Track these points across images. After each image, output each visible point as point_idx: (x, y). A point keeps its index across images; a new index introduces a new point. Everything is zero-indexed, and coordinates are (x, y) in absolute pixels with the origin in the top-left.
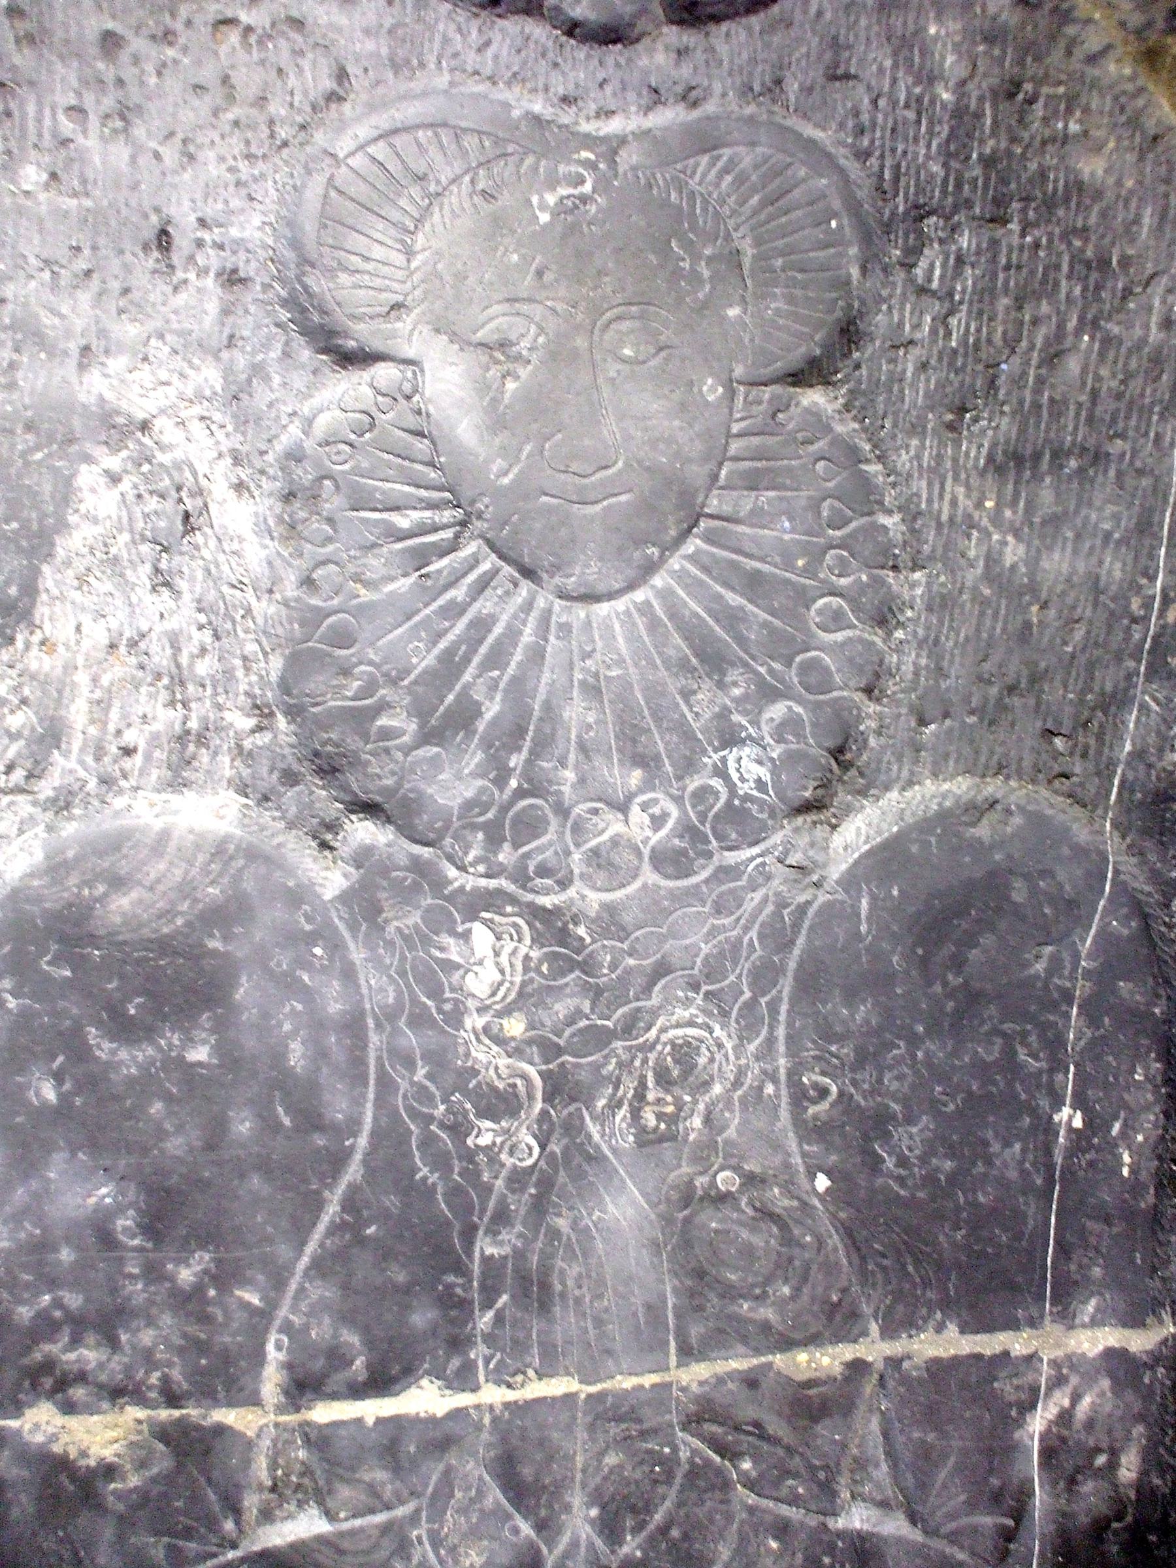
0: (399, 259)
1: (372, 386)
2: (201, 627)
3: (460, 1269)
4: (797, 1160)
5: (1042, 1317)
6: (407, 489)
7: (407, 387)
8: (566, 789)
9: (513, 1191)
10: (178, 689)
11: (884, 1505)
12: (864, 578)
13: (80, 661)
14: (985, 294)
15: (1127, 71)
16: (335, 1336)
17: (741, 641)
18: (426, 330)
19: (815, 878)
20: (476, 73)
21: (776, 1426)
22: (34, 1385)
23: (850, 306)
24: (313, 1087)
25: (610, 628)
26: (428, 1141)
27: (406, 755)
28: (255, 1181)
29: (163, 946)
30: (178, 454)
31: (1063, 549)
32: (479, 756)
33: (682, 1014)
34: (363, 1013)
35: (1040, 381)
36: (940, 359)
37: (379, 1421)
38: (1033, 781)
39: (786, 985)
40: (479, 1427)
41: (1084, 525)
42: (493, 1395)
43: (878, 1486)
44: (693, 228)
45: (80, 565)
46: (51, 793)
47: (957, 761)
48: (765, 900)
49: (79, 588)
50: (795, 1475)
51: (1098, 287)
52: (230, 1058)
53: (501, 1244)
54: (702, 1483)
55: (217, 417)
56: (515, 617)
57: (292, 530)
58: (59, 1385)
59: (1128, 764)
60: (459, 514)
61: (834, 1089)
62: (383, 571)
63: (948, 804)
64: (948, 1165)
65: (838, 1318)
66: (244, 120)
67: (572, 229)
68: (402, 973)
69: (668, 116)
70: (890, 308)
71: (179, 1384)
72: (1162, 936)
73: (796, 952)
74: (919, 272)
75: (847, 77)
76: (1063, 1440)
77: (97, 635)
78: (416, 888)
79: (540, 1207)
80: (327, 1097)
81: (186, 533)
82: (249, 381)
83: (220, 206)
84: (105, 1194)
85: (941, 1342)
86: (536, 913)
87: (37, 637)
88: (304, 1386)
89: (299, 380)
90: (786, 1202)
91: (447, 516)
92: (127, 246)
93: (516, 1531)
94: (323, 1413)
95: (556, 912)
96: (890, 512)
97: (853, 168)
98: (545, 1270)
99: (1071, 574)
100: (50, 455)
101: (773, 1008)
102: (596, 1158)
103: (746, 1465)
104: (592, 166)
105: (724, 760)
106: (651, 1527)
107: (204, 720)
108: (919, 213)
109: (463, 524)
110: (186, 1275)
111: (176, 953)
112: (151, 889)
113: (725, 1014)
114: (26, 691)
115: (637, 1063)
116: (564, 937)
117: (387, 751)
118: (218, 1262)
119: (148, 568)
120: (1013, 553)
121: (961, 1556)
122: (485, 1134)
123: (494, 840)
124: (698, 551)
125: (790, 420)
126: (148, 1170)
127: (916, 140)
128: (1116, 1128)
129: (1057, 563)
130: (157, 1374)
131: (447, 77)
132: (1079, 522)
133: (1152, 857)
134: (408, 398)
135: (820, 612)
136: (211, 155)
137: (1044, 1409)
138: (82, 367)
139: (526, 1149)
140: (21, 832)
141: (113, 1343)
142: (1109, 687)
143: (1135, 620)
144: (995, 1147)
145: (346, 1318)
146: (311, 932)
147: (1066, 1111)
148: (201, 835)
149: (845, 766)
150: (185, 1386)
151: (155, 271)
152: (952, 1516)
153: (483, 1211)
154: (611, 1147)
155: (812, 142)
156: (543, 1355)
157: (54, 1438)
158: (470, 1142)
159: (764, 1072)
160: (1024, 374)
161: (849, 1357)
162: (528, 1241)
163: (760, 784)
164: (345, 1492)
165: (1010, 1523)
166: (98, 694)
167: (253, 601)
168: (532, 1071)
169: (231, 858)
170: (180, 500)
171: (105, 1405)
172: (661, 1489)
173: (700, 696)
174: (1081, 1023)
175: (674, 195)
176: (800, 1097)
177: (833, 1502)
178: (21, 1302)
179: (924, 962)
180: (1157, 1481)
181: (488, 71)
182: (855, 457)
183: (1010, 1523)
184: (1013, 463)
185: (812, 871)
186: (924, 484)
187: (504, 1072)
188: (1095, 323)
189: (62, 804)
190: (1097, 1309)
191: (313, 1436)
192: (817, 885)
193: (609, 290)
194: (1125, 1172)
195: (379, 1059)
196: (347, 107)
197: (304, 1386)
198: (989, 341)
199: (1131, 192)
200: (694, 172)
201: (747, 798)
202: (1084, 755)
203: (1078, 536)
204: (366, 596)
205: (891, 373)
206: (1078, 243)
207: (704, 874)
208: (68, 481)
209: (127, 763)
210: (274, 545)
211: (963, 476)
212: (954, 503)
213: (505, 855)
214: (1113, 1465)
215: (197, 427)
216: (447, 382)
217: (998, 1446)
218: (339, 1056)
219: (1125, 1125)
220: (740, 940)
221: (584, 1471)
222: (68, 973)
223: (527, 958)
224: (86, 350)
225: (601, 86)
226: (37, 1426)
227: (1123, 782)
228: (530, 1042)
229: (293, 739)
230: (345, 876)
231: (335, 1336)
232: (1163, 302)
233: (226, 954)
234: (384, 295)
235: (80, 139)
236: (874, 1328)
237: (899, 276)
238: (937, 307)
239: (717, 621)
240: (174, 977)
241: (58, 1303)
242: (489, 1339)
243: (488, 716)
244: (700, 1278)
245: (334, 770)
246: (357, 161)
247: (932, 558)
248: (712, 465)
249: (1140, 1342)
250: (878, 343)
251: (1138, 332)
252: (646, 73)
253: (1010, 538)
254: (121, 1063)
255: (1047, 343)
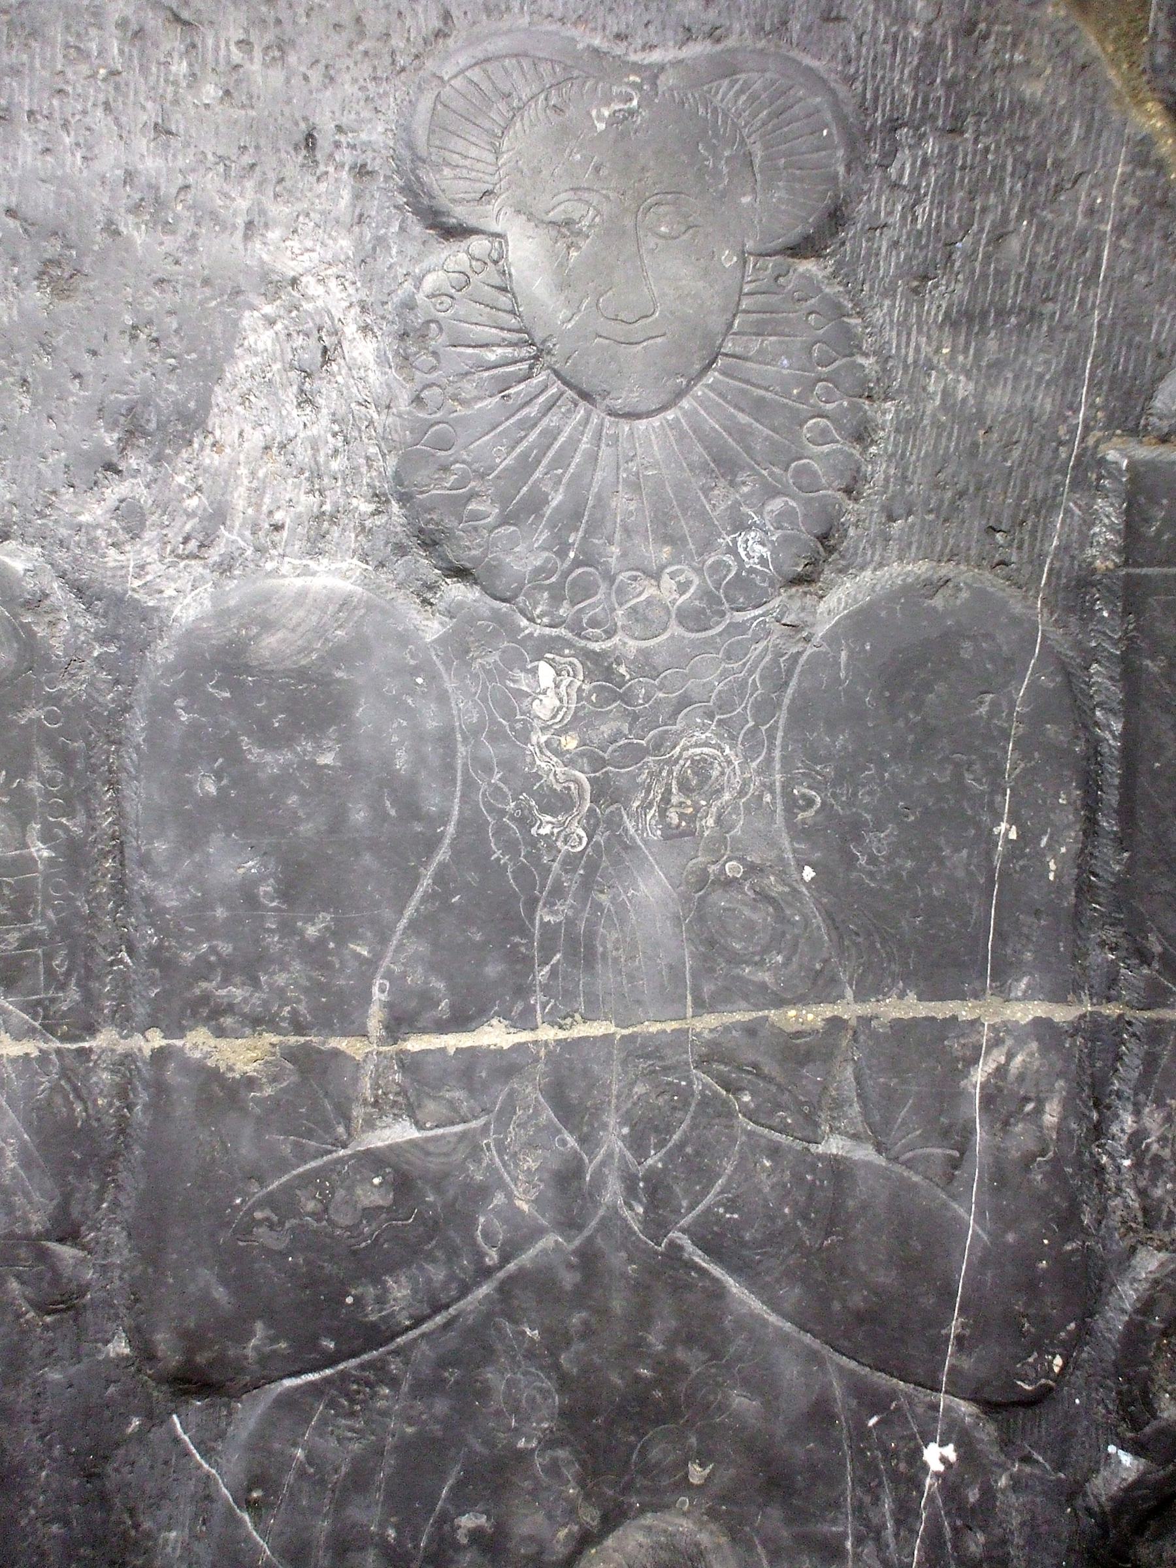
0: (491, 158)
1: (467, 252)
2: (335, 435)
3: (524, 932)
4: (789, 855)
5: (984, 990)
6: (494, 330)
7: (495, 255)
8: (613, 561)
9: (567, 871)
10: (316, 481)
11: (855, 1137)
12: (845, 404)
13: (242, 458)
14: (946, 187)
15: (1062, 13)
16: (426, 983)
17: (748, 450)
18: (510, 210)
19: (805, 634)
20: (550, 15)
21: (770, 1067)
22: (194, 1014)
23: (837, 196)
24: (412, 785)
25: (648, 437)
26: (501, 830)
27: (491, 532)
28: (367, 859)
29: (302, 674)
30: (320, 303)
31: (1005, 385)
32: (546, 534)
33: (700, 736)
34: (453, 729)
35: (988, 257)
36: (908, 239)
37: (459, 1051)
38: (979, 566)
39: (782, 716)
40: (537, 1060)
41: (1021, 369)
42: (548, 1034)
43: (852, 1123)
44: (716, 135)
45: (243, 386)
46: (217, 558)
47: (918, 548)
48: (766, 649)
49: (243, 404)
50: (785, 1108)
51: (1035, 184)
52: (351, 765)
53: (556, 913)
54: (710, 1110)
55: (350, 276)
56: (575, 428)
57: (405, 361)
58: (214, 1015)
59: (1056, 555)
60: (533, 350)
61: (818, 799)
62: (475, 393)
63: (910, 580)
64: (909, 864)
65: (820, 982)
66: (372, 52)
67: (623, 135)
68: (484, 700)
69: (697, 49)
70: (869, 200)
71: (304, 1016)
72: (1082, 691)
73: (790, 691)
74: (893, 171)
75: (838, 19)
76: (1000, 1090)
77: (256, 438)
78: (495, 634)
79: (587, 885)
80: (424, 793)
81: (325, 363)
82: (374, 249)
83: (353, 116)
84: (252, 865)
85: (903, 1006)
86: (588, 656)
87: (209, 441)
88: (399, 1023)
89: (412, 249)
90: (780, 888)
91: (524, 352)
92: (281, 144)
93: (564, 1143)
94: (415, 1044)
95: (603, 654)
96: (866, 355)
97: (842, 91)
98: (591, 934)
99: (1010, 406)
100: (222, 303)
101: (771, 737)
102: (630, 848)
103: (746, 1098)
104: (638, 87)
105: (734, 541)
106: (670, 1144)
107: (336, 504)
108: (893, 125)
109: (536, 358)
110: (312, 931)
111: (311, 681)
112: (293, 630)
113: (733, 738)
114: (201, 482)
115: (664, 774)
116: (608, 673)
117: (475, 529)
118: (336, 920)
119: (295, 388)
120: (964, 388)
121: (916, 1179)
122: (546, 826)
123: (557, 598)
124: (716, 381)
125: (790, 283)
126: (284, 848)
127: (892, 69)
128: (1044, 841)
129: (1000, 397)
130: (288, 1008)
131: (527, 19)
132: (1017, 366)
133: (1074, 629)
134: (496, 262)
135: (810, 430)
136: (347, 77)
137: (985, 1064)
138: (247, 238)
139: (578, 839)
140: (194, 588)
141: (255, 983)
142: (1040, 495)
143: (1061, 443)
144: (946, 852)
145: (434, 967)
146: (415, 667)
147: (1003, 826)
148: (332, 591)
149: (830, 550)
150: (309, 1018)
151: (303, 165)
152: (910, 1147)
153: (543, 886)
154: (642, 839)
155: (809, 70)
156: (588, 1003)
157: (208, 1055)
158: (533, 831)
159: (763, 784)
160: (975, 251)
161: (829, 1015)
162: (578, 912)
163: (763, 561)
164: (431, 1106)
165: (956, 1154)
166: (255, 484)
167: (375, 416)
168: (582, 777)
169: (355, 608)
170: (320, 338)
171: (248, 1031)
172: (679, 1115)
173: (716, 492)
174: (1016, 755)
175: (701, 111)
176: (792, 805)
177: (815, 1132)
178: (186, 949)
179: (891, 702)
180: (1074, 1126)
181: (558, 14)
182: (839, 312)
183: (956, 1154)
184: (965, 320)
185: (803, 629)
186: (894, 333)
187: (561, 778)
188: (1032, 210)
189: (225, 567)
190: (1028, 986)
191: (407, 1061)
192: (807, 640)
193: (650, 181)
194: (1051, 877)
195: (465, 764)
196: (450, 42)
197: (399, 1023)
198: (947, 224)
199: (1064, 108)
200: (717, 93)
201: (752, 571)
202: (1020, 548)
203: (1016, 377)
204: (461, 411)
205: (869, 249)
206: (1020, 149)
207: (719, 629)
208: (235, 323)
209: (276, 537)
210: (393, 373)
211: (925, 329)
212: (918, 349)
213: (564, 611)
214: (1039, 1111)
215: (333, 284)
216: (525, 250)
217: (947, 1092)
218: (435, 762)
219: (1051, 838)
220: (745, 680)
221: (618, 1097)
222: (228, 695)
223: (580, 689)
224: (250, 224)
225: (646, 25)
226: (196, 1046)
227: (1051, 570)
228: (582, 755)
229: (404, 520)
230: (441, 623)
231: (426, 983)
232: (1089, 195)
233: (349, 681)
234: (478, 185)
235: (247, 65)
236: (849, 993)
237: (877, 175)
238: (907, 198)
239: (730, 434)
240: (311, 699)
241: (213, 950)
242: (546, 989)
243: (554, 504)
244: (711, 945)
245: (435, 543)
246: (458, 83)
247: (899, 391)
248: (729, 316)
249: (1062, 1014)
250: (859, 225)
251: (1067, 218)
252: (680, 15)
253: (962, 378)
254: (265, 764)
255: (994, 226)
